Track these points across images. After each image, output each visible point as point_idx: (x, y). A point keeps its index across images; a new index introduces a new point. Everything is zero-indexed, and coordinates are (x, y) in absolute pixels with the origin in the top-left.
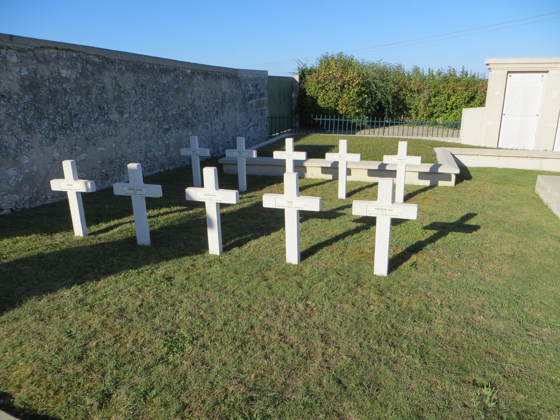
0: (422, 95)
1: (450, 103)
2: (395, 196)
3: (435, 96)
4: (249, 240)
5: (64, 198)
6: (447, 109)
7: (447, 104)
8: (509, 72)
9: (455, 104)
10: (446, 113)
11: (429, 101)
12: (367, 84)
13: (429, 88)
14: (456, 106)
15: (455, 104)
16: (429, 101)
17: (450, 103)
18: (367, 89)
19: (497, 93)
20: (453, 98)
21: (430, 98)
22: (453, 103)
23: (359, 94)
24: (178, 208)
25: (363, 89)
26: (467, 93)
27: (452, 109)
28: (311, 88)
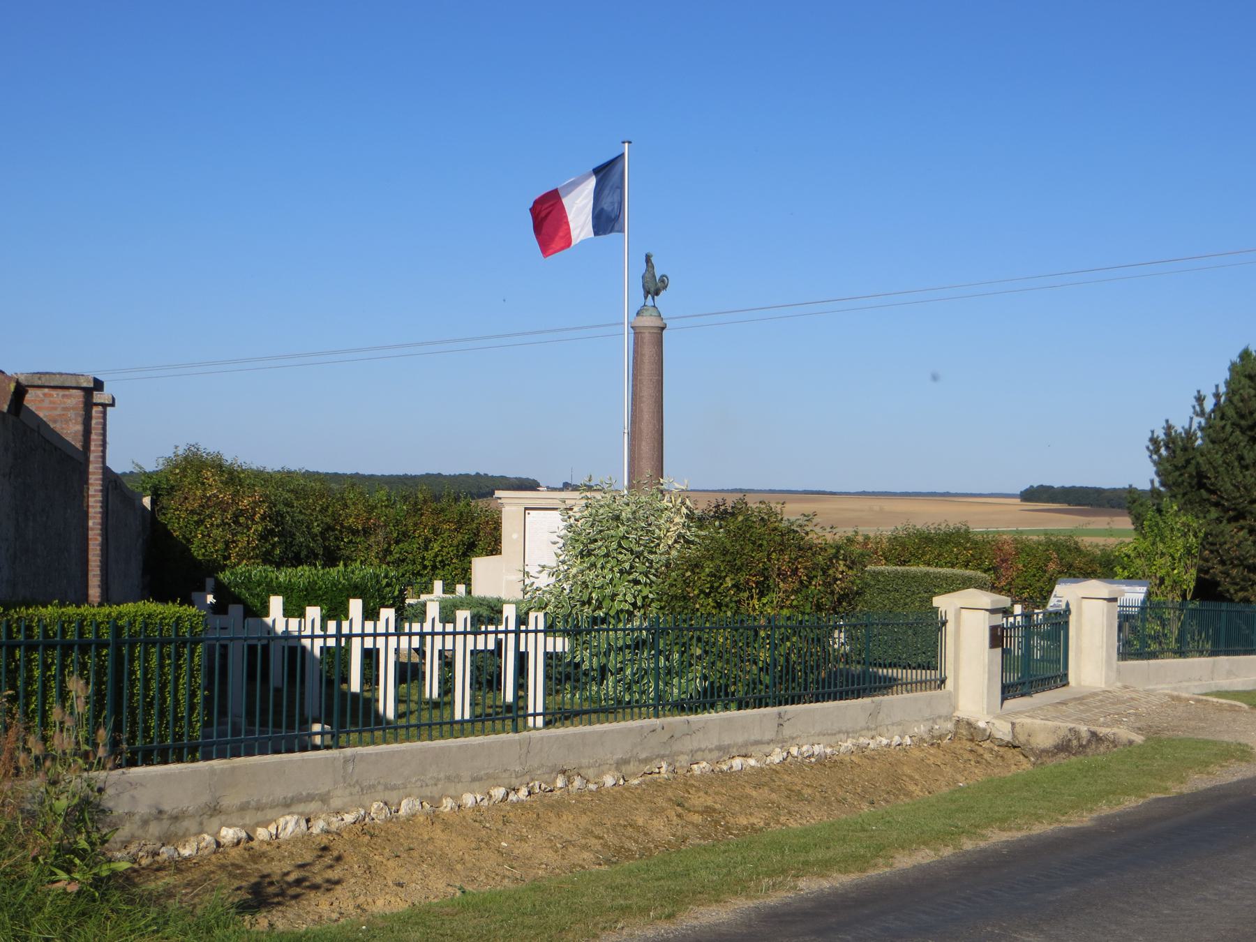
0: (372, 539)
1: (429, 555)
2: (1098, 492)
3: (397, 542)
4: (966, 583)
5: (297, 748)
6: (425, 567)
7: (423, 558)
8: (526, 509)
9: (439, 558)
10: (421, 575)
11: (388, 552)
12: (277, 518)
13: (386, 526)
14: (442, 561)
15: (439, 558)
16: (388, 552)
17: (429, 555)
18: (277, 526)
19: (515, 536)
20: (436, 547)
21: (390, 545)
22: (436, 556)
23: (264, 537)
24: (1065, 506)
25: (270, 526)
26: (460, 537)
27: (434, 568)
28: (176, 521)
